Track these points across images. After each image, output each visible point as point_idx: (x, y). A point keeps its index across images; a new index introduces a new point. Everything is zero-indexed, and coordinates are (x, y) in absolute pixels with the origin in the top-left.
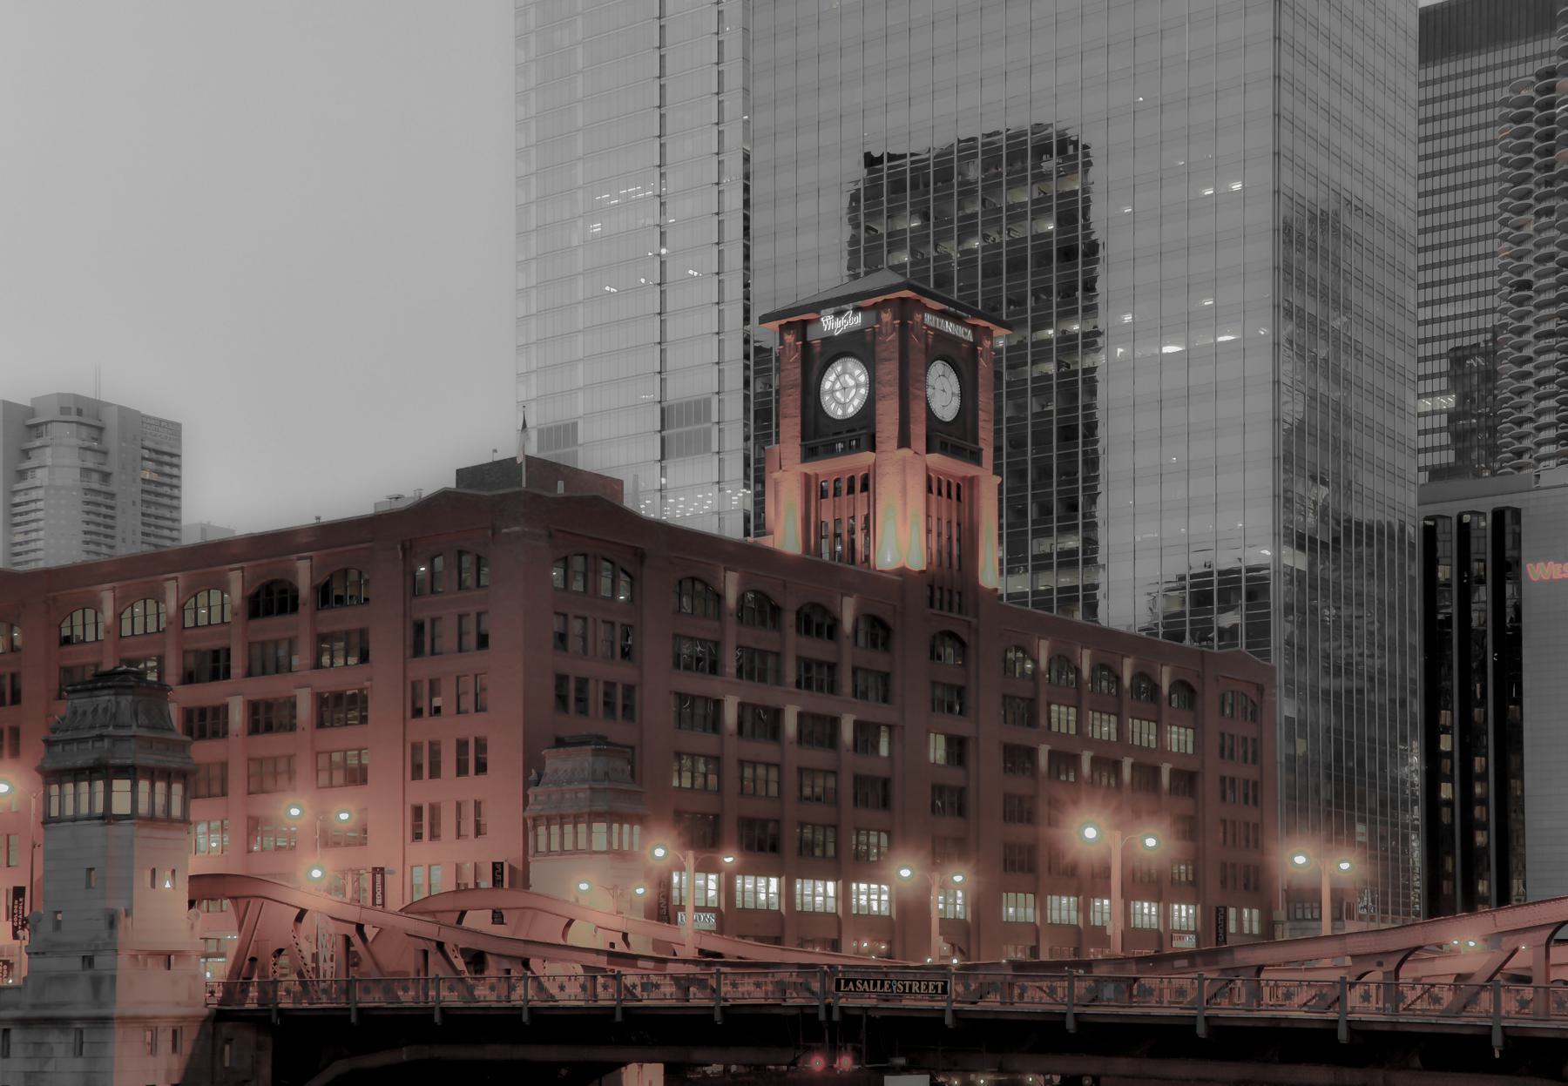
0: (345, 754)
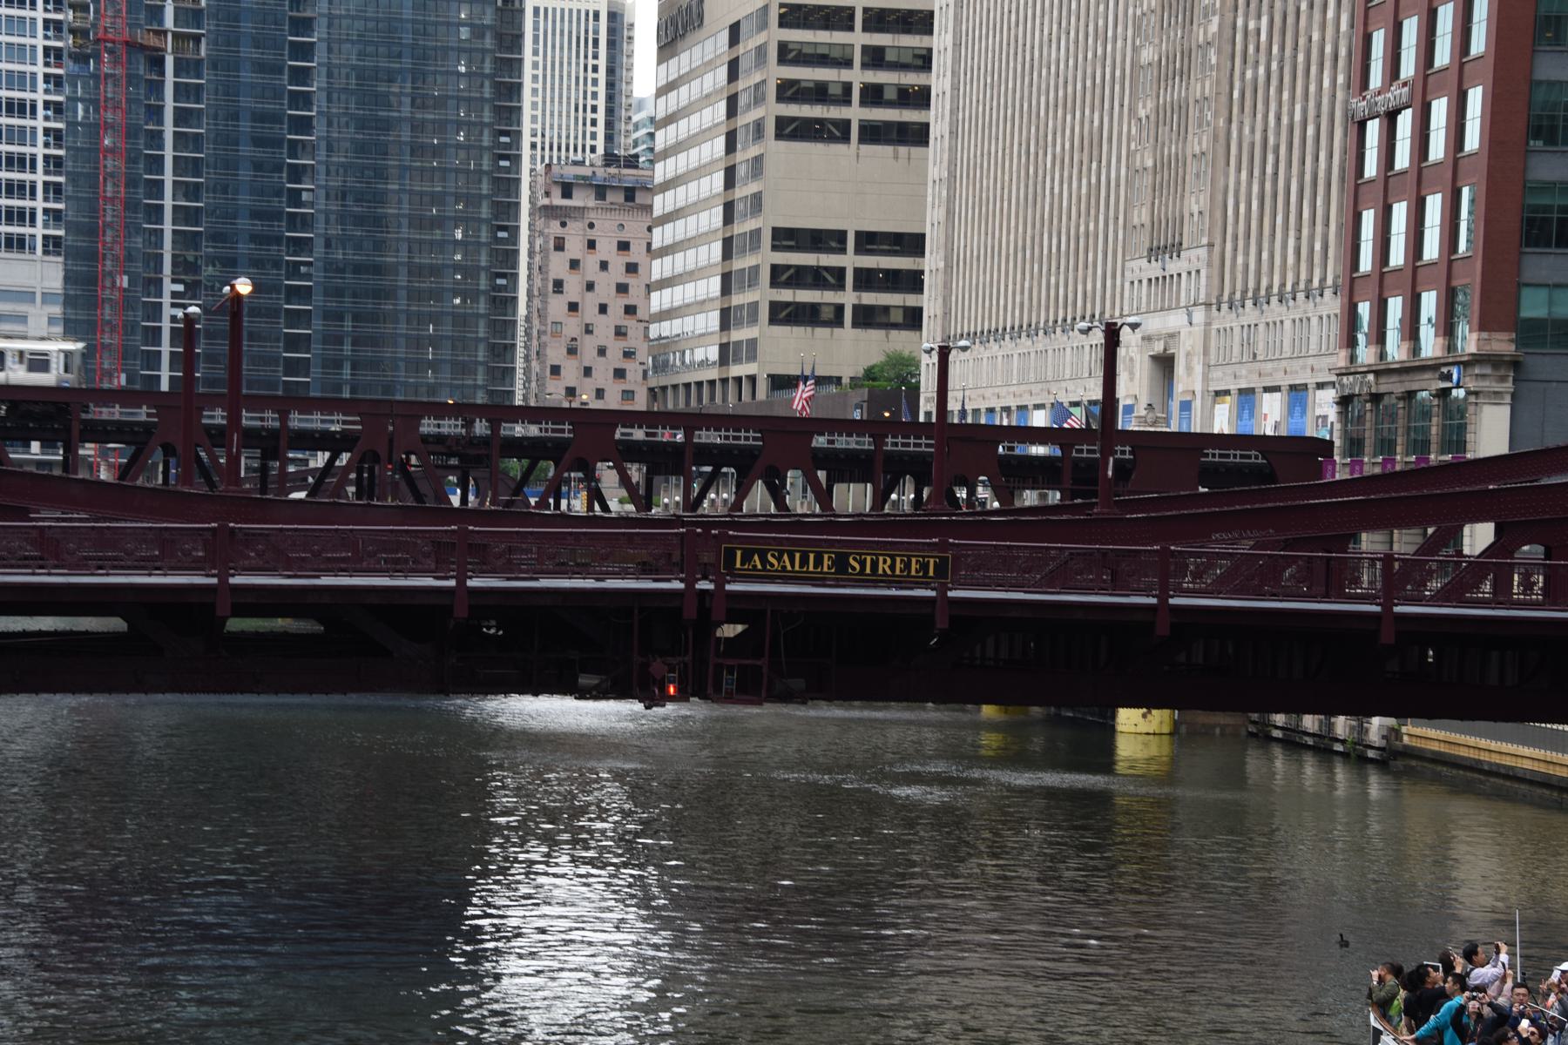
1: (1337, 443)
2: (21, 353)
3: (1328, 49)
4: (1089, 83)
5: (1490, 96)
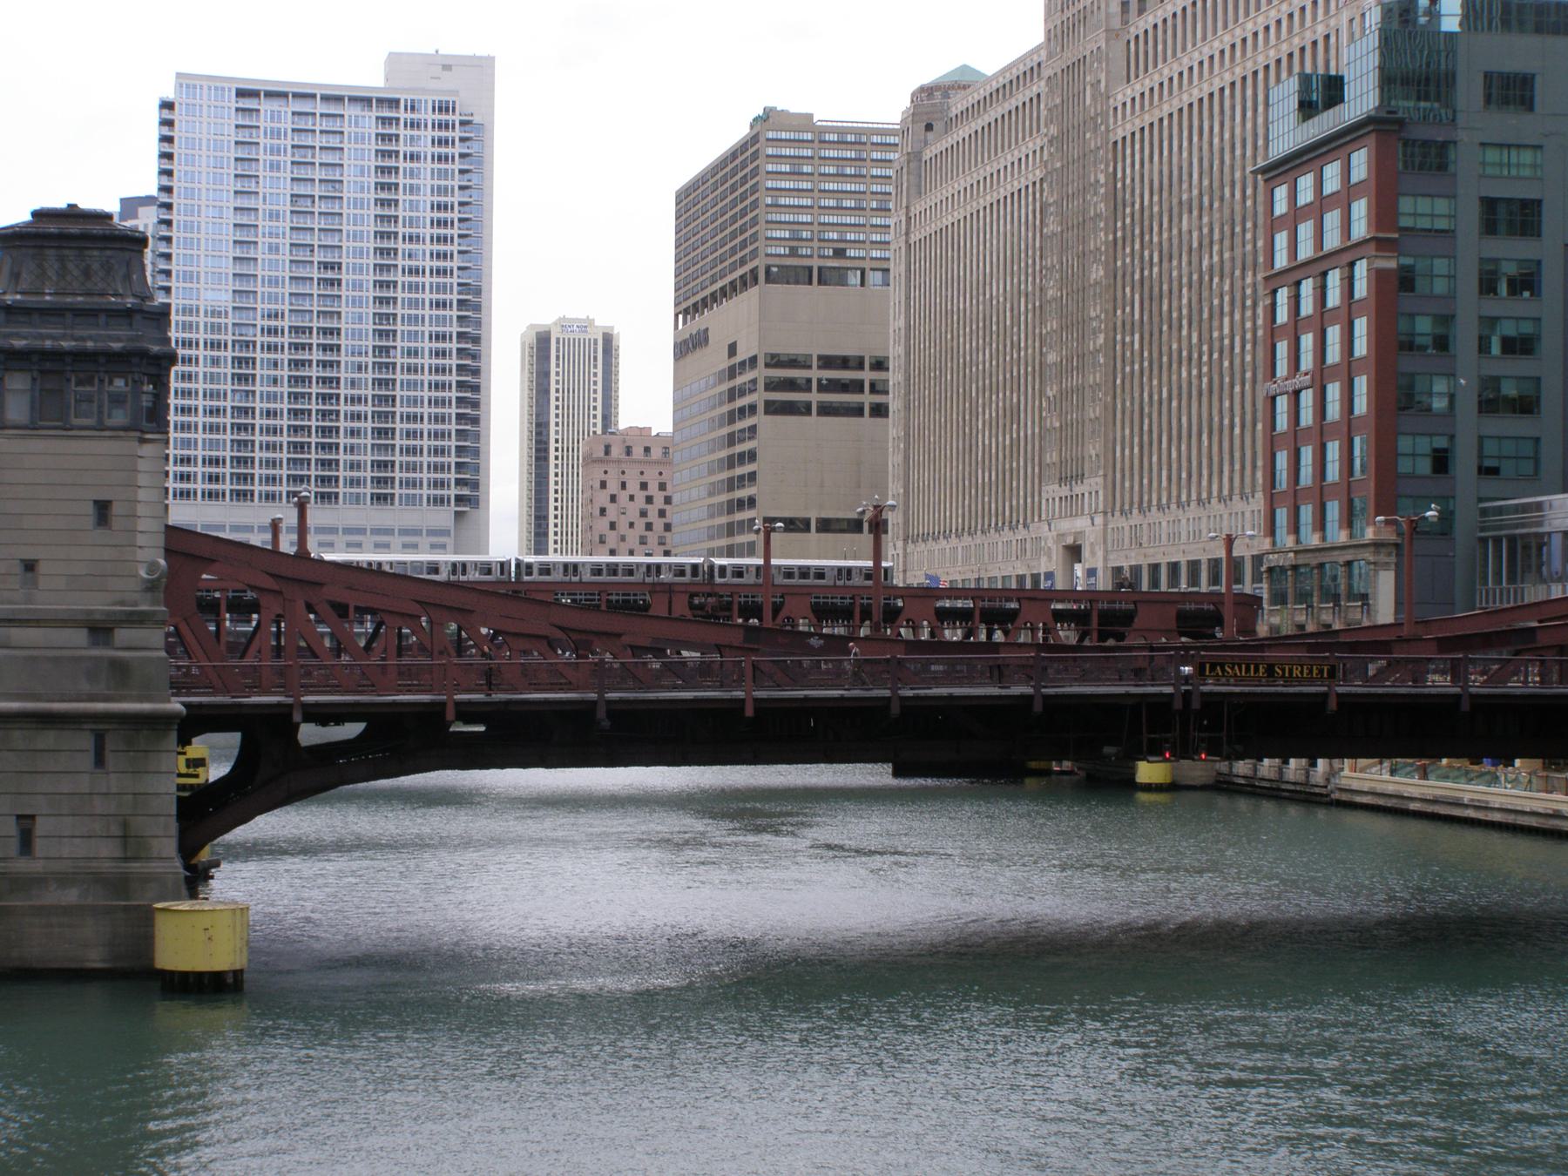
0: (100, 421)
1: (1265, 596)
2: (476, 563)
3: (1185, 354)
4: (1008, 376)
5: (1373, 383)
